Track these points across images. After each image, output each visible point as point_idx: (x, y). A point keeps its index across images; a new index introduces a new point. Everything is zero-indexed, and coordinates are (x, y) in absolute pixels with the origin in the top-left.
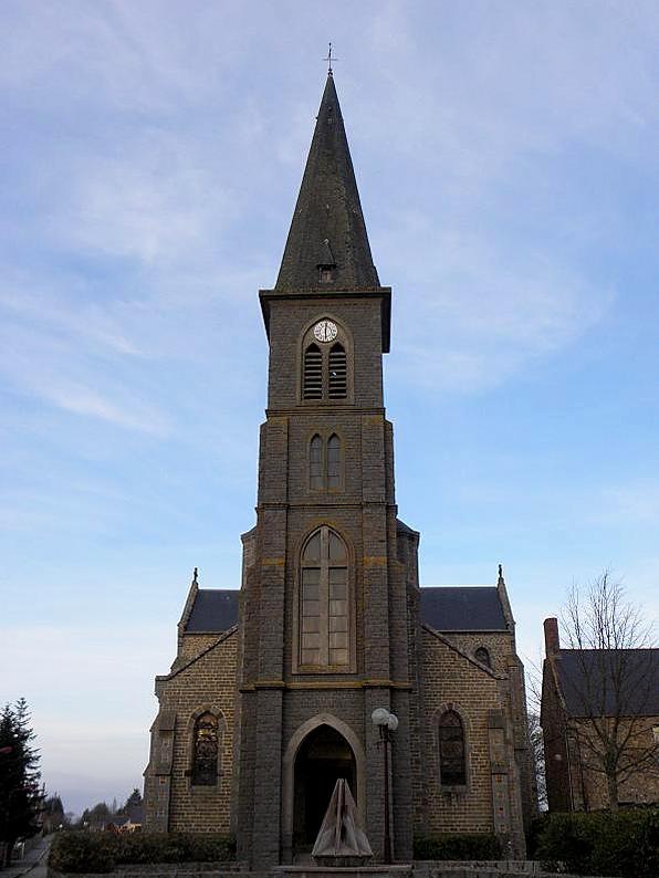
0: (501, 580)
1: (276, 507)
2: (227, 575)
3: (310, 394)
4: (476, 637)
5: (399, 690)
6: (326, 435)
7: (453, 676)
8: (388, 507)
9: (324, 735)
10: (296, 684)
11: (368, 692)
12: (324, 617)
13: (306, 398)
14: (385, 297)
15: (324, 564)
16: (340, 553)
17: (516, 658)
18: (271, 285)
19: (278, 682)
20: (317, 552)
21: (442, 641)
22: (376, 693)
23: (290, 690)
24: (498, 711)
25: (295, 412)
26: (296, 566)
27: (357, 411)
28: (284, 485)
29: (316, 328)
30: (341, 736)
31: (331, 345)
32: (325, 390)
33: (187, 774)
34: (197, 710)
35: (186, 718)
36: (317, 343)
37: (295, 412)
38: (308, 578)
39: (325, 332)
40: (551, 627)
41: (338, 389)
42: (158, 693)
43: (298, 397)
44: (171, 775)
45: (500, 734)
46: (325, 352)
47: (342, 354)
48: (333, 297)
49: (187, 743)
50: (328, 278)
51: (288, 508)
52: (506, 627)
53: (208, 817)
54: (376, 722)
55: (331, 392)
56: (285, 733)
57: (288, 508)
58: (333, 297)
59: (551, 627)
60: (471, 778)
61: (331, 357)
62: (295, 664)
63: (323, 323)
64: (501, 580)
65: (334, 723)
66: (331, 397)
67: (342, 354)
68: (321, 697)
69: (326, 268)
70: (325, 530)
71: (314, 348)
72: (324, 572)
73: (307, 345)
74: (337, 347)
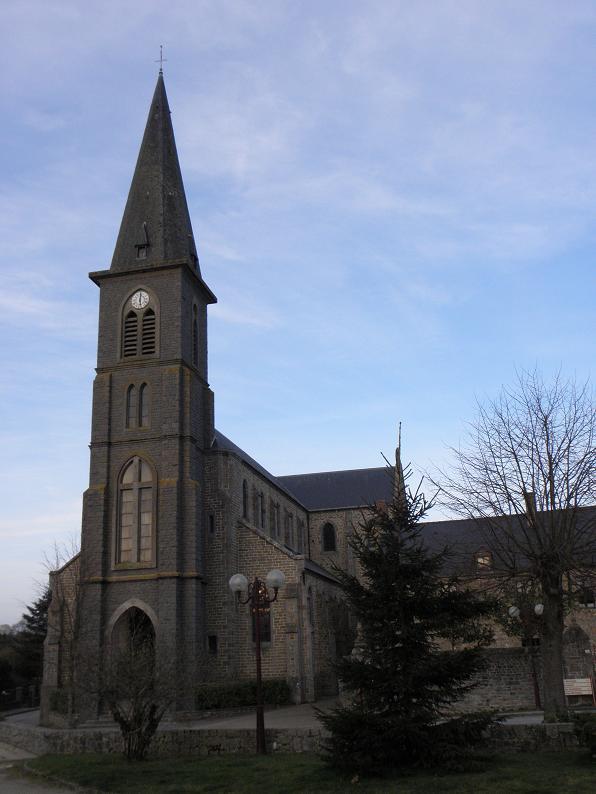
2: (210, 307)
3: (128, 352)
5: (186, 578)
7: (263, 559)
10: (114, 578)
11: (161, 581)
13: (126, 356)
21: (255, 533)
22: (166, 582)
23: (110, 583)
24: (295, 585)
26: (115, 489)
27: (161, 363)
28: (107, 427)
32: (139, 348)
36: (135, 311)
39: (140, 300)
43: (118, 355)
44: (59, 643)
45: (294, 603)
46: (140, 317)
48: (144, 271)
50: (143, 255)
51: (109, 444)
53: (591, 672)
54: (234, 589)
55: (144, 349)
56: (105, 615)
57: (109, 444)
58: (144, 271)
60: (274, 637)
61: (144, 321)
62: (113, 564)
63: (138, 293)
65: (140, 605)
66: (144, 354)
68: (131, 587)
69: (140, 247)
71: (132, 314)
73: (126, 312)
74: (149, 312)
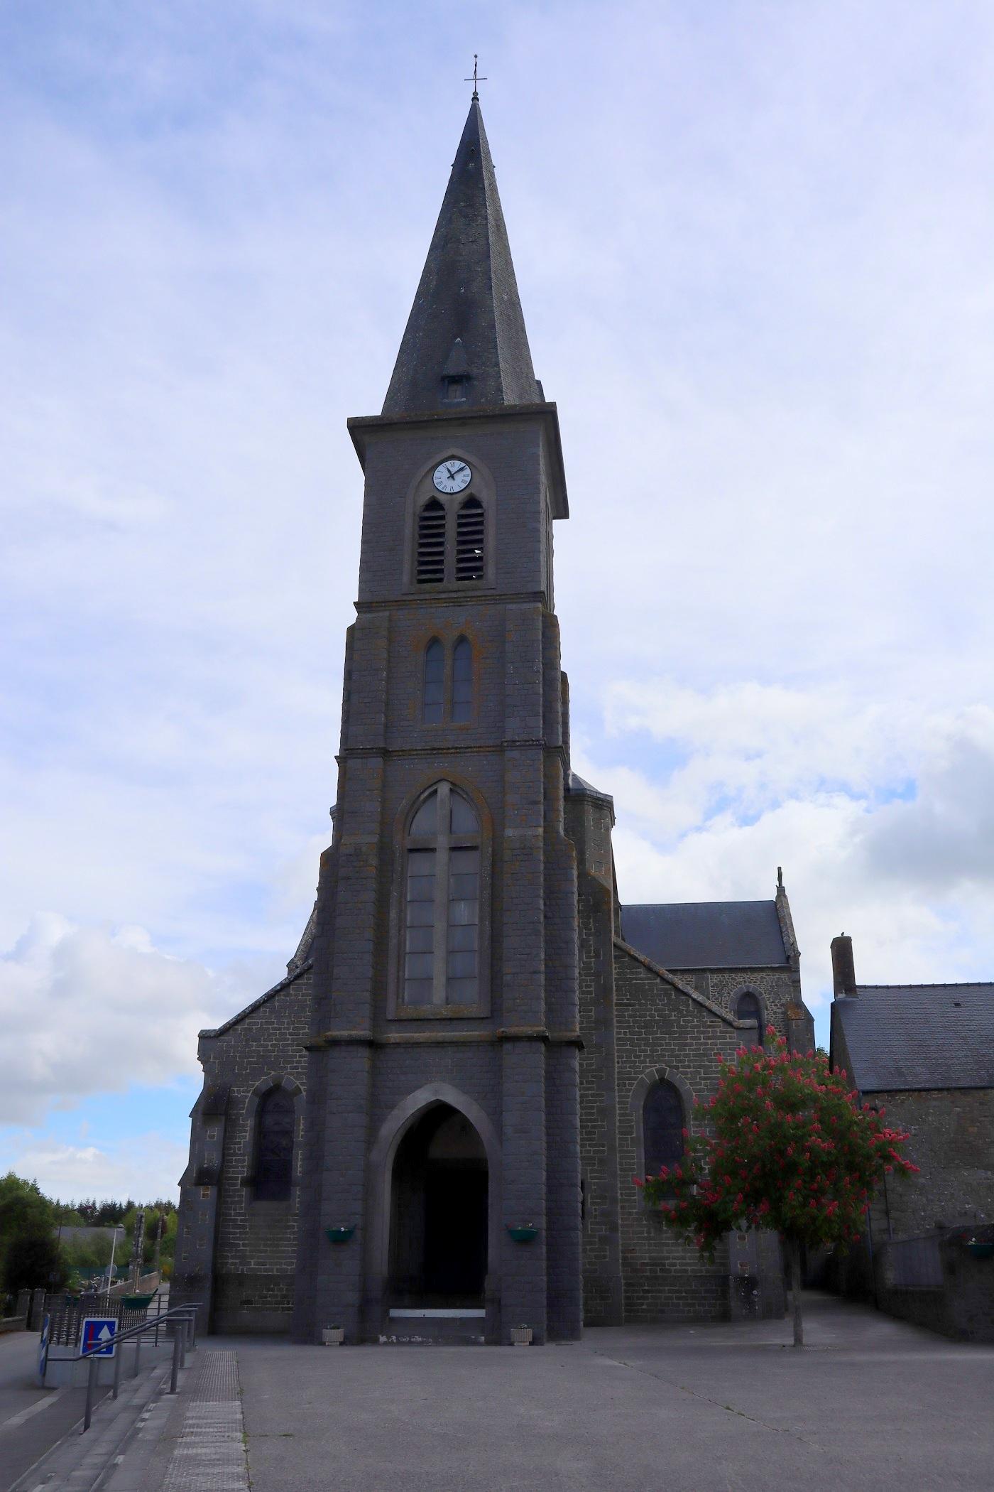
0: (781, 890)
1: (366, 753)
3: (429, 569)
4: (739, 977)
6: (449, 637)
8: (352, 659)
9: (439, 1114)
12: (440, 927)
14: (548, 414)
15: (442, 842)
16: (467, 822)
17: (800, 1005)
18: (373, 406)
19: (363, 1032)
20: (429, 823)
25: (400, 604)
29: (437, 474)
30: (468, 1121)
31: (461, 497)
33: (245, 1182)
34: (261, 1083)
35: (245, 1095)
36: (441, 498)
37: (400, 604)
38: (418, 865)
40: (842, 950)
41: (471, 568)
42: (203, 1056)
47: (479, 511)
49: (245, 1136)
52: (789, 963)
56: (376, 1109)
59: (842, 950)
64: (781, 890)
65: (452, 1097)
67: (479, 511)
70: (444, 789)
71: (434, 504)
72: (442, 856)
73: (424, 499)
74: (472, 501)
